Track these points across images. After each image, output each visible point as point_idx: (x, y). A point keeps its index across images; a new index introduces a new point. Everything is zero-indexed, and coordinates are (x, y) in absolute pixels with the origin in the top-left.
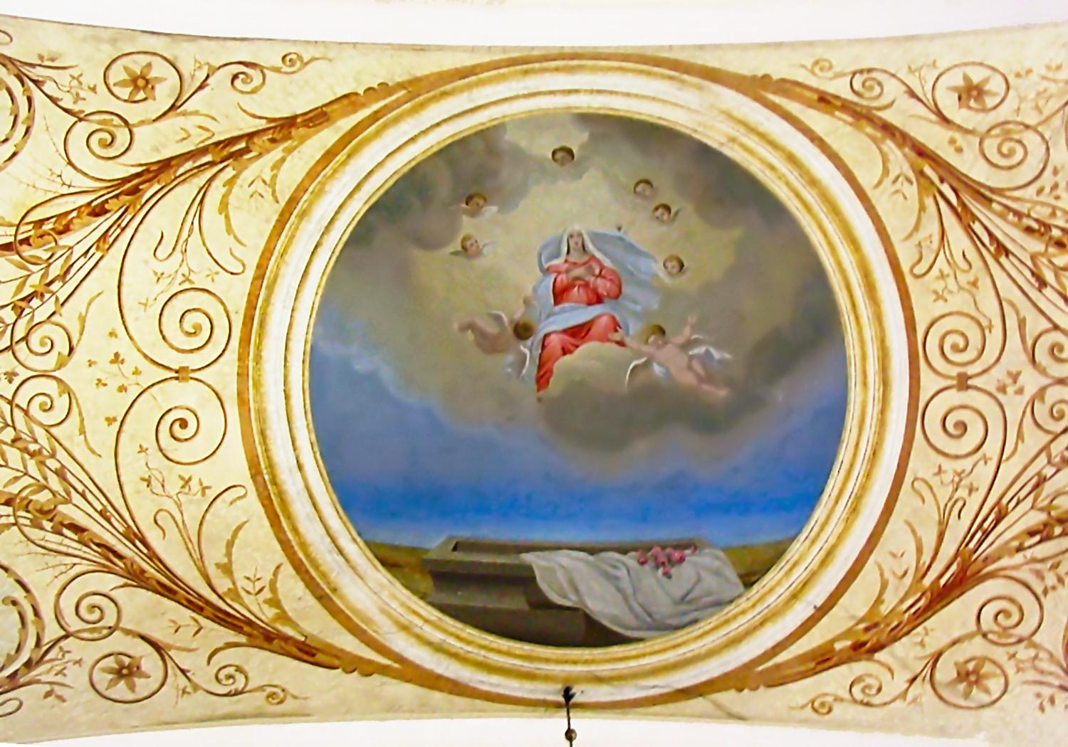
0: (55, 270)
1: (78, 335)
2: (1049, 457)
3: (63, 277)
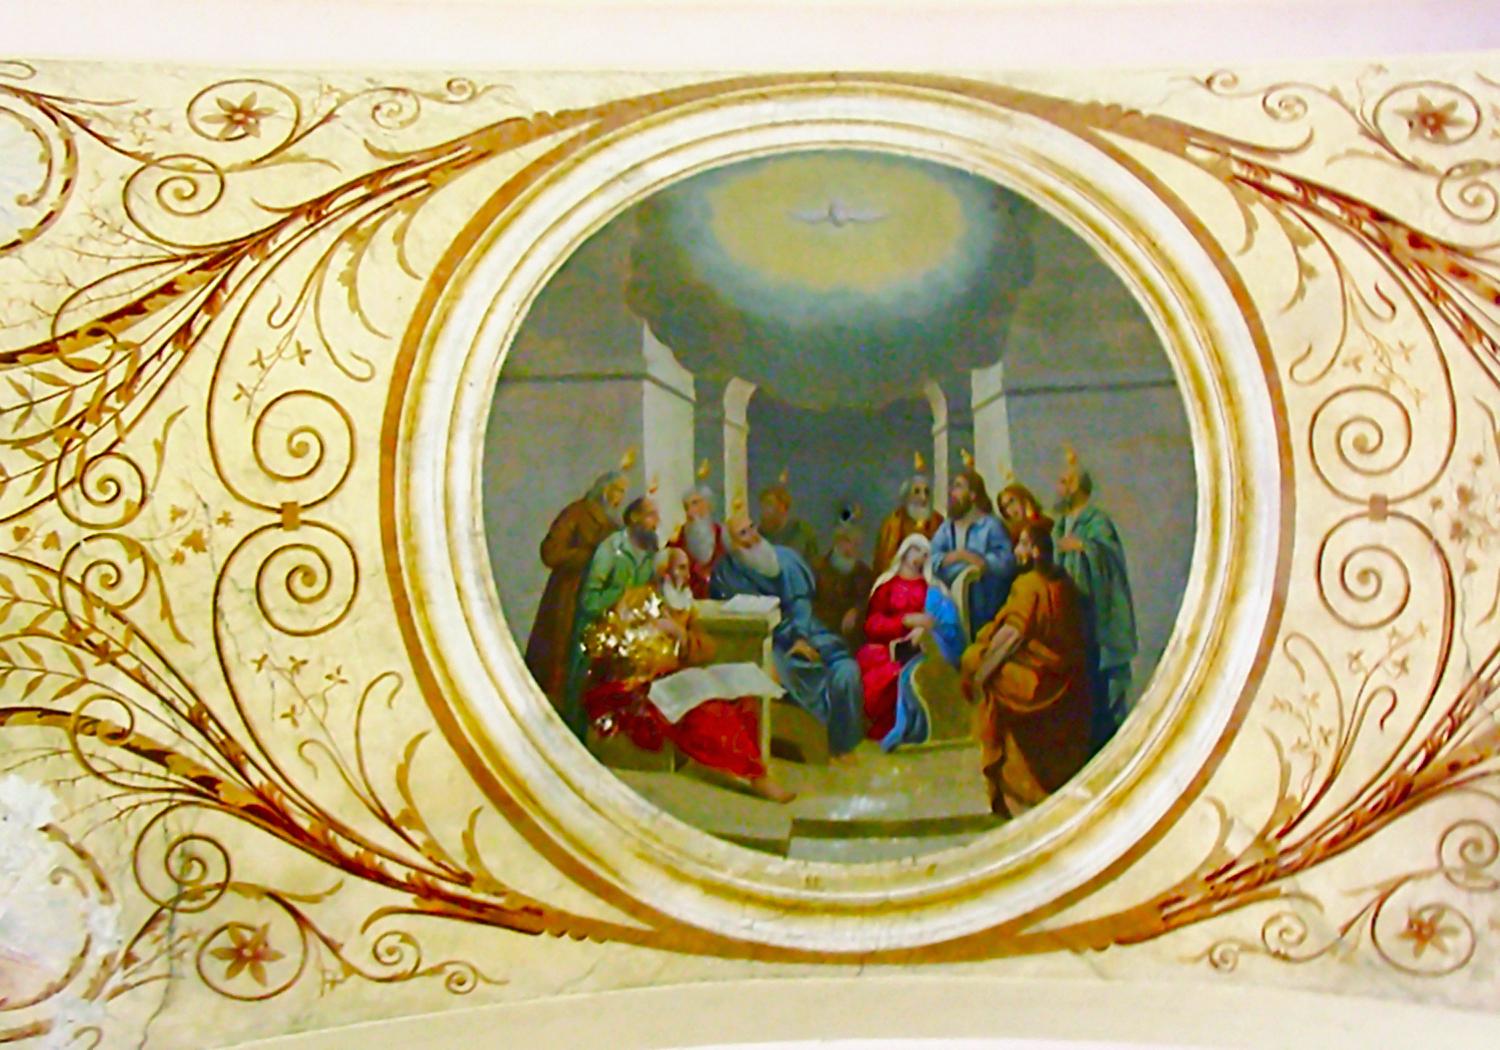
0: (117, 375)
1: (154, 466)
2: (118, 423)
3: (126, 389)
